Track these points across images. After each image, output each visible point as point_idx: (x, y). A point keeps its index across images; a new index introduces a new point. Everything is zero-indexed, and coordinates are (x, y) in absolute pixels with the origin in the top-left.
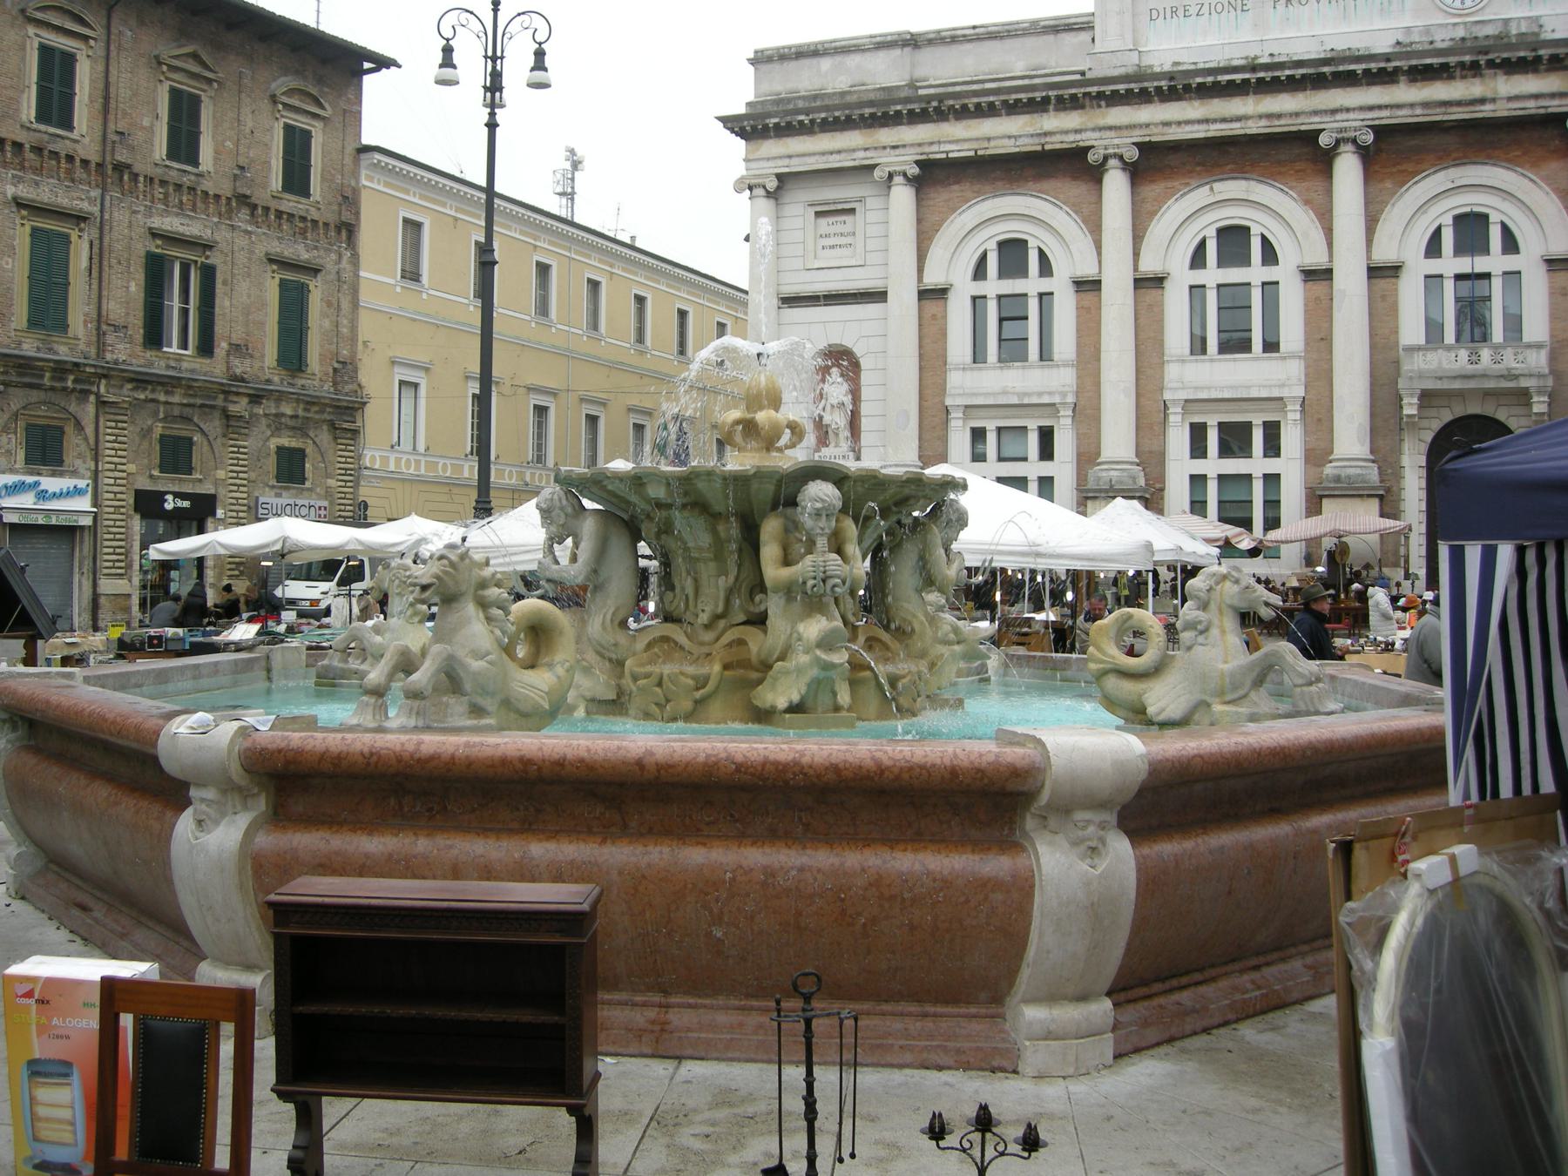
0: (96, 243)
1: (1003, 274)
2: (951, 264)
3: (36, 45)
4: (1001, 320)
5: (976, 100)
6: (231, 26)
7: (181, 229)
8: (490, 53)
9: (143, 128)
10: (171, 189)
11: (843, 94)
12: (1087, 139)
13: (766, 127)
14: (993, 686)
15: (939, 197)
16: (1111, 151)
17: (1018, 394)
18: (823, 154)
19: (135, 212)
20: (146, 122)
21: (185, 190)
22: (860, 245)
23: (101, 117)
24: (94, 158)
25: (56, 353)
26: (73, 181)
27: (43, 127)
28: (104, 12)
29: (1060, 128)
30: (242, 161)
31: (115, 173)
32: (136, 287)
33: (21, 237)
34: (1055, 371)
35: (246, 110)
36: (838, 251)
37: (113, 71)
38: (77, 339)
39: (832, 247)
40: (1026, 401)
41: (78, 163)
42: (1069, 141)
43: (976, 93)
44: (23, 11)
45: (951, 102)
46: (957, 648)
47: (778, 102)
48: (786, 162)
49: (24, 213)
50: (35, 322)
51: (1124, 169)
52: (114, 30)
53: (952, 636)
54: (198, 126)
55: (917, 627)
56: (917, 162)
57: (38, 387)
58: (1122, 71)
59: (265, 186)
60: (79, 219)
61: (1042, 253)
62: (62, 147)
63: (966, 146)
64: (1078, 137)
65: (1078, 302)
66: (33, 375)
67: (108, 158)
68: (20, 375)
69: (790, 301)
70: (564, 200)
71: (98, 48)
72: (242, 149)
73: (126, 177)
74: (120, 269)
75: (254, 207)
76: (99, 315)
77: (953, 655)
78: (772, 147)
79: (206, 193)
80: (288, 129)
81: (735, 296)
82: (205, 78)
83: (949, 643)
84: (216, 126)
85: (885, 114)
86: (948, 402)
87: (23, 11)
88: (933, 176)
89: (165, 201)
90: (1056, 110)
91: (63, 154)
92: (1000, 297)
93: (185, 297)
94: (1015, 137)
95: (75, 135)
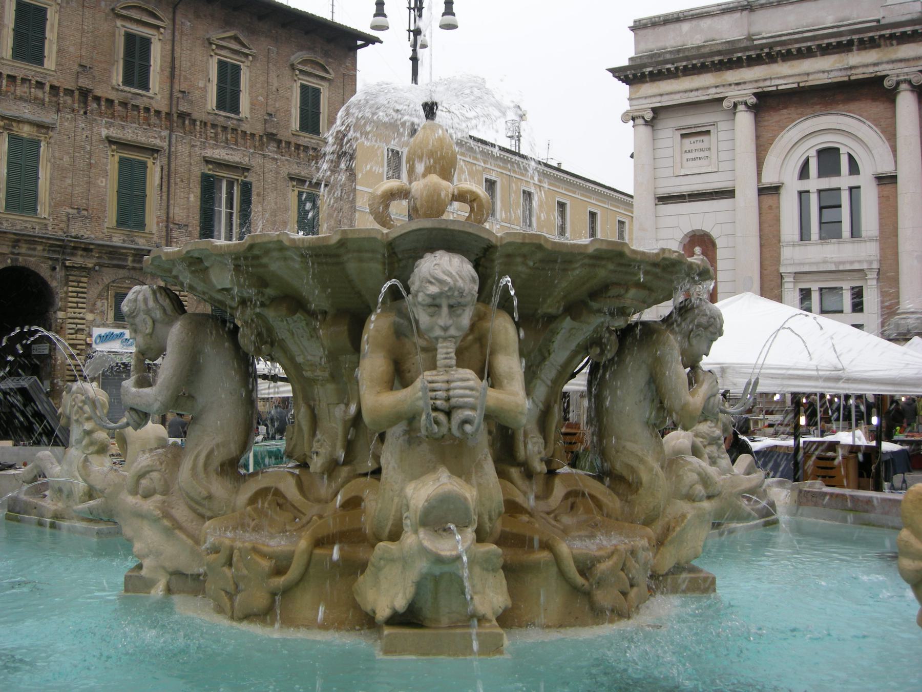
0: (166, 167)
1: (822, 174)
2: (782, 167)
3: (123, 33)
4: (821, 208)
5: (797, 46)
6: (261, 18)
7: (227, 157)
8: (413, 5)
10: (219, 130)
11: (699, 47)
12: (882, 70)
13: (643, 74)
14: (783, 535)
15: (772, 119)
16: (902, 78)
17: (835, 263)
18: (685, 92)
19: (193, 146)
20: (201, 85)
21: (230, 131)
22: (714, 157)
23: (169, 80)
24: (164, 109)
25: (137, 244)
26: (149, 125)
27: (127, 89)
28: (171, 10)
29: (862, 63)
30: (270, 110)
31: (179, 119)
32: (194, 198)
33: (112, 162)
34: (863, 244)
35: (273, 75)
36: (698, 162)
37: (178, 49)
38: (151, 233)
39: (695, 159)
40: (841, 268)
41: (152, 113)
42: (869, 72)
43: (797, 41)
44: (113, 10)
45: (779, 49)
46: (706, 505)
47: (652, 56)
48: (659, 99)
49: (114, 147)
50: (122, 222)
51: (912, 91)
52: (178, 22)
53: (699, 489)
55: (645, 477)
56: (755, 94)
57: (123, 267)
58: (908, 17)
59: (287, 127)
60: (154, 151)
61: (851, 157)
62: (141, 102)
64: (876, 69)
65: (879, 193)
66: (120, 259)
67: (174, 110)
68: (111, 259)
69: (665, 199)
71: (168, 35)
72: (270, 102)
73: (187, 122)
74: (181, 185)
75: (280, 142)
76: (168, 217)
77: (700, 516)
78: (648, 89)
79: (244, 133)
80: (304, 88)
81: (623, 199)
82: (243, 53)
83: (690, 498)
84: (251, 87)
85: (730, 60)
86: (782, 270)
87: (113, 10)
88: (767, 103)
89: (216, 138)
90: (859, 49)
91: (142, 106)
92: (820, 191)
93: (230, 205)
94: (828, 72)
95: (151, 93)
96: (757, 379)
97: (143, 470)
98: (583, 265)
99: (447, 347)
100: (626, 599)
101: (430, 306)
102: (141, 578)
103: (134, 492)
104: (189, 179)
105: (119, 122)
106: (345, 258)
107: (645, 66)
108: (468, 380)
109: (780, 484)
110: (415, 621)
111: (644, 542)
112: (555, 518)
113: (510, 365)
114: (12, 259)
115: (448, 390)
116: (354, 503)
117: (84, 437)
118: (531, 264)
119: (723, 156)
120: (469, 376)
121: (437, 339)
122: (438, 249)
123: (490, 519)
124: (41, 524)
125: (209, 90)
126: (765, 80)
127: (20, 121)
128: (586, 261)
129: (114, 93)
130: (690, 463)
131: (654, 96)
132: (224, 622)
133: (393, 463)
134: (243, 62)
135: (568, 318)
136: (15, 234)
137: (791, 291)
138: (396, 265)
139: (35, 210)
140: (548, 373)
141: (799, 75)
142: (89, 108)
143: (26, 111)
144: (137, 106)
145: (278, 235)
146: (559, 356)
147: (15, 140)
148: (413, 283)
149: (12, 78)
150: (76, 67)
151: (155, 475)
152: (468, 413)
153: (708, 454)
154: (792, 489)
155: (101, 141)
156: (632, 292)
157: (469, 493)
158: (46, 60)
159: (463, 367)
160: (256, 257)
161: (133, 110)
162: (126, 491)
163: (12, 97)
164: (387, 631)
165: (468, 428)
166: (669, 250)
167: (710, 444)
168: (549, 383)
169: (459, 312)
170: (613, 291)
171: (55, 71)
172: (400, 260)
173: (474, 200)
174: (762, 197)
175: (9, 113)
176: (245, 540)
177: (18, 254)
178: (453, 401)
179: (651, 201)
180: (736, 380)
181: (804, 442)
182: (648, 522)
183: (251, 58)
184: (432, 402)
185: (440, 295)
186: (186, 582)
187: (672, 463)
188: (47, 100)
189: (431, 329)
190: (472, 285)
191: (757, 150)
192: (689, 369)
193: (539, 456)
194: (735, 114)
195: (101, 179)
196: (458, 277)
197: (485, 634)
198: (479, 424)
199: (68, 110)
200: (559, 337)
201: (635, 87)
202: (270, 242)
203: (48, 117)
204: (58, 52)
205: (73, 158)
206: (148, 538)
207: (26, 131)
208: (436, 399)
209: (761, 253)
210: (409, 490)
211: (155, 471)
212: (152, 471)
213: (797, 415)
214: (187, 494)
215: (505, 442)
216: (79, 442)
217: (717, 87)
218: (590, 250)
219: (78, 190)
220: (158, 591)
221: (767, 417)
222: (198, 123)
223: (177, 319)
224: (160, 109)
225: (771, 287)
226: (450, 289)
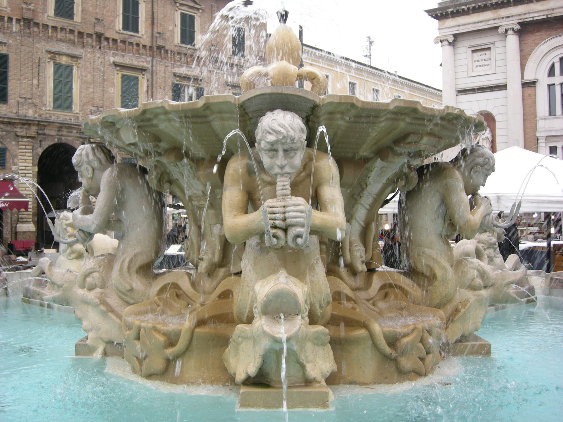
0: (150, 80)
2: (537, 70)
9: (169, 31)
14: (539, 308)
15: (530, 39)
18: (474, 23)
20: (171, 28)
23: (150, 26)
24: (148, 44)
26: (139, 54)
27: (125, 32)
31: (158, 50)
33: (117, 77)
36: (483, 68)
41: (141, 46)
46: (484, 293)
48: (457, 28)
49: (118, 68)
53: (478, 281)
54: (193, 28)
55: (439, 273)
60: (142, 70)
62: (134, 40)
63: (542, 14)
67: (154, 44)
70: (367, 58)
73: (162, 52)
77: (480, 301)
83: (473, 288)
86: (538, 135)
88: (526, 29)
91: (135, 43)
96: (520, 202)
97: (88, 271)
98: (387, 119)
99: (284, 181)
100: (424, 364)
101: (270, 150)
102: (86, 345)
103: (83, 287)
104: (165, 87)
105: (120, 53)
106: (211, 118)
107: (448, 7)
108: (299, 205)
109: (538, 274)
110: (264, 382)
111: (438, 322)
112: (374, 304)
113: (333, 193)
114: (58, 139)
115: (284, 213)
116: (226, 295)
117: (68, 248)
118: (348, 119)
119: (499, 63)
120: (300, 202)
121: (276, 175)
122: (276, 109)
123: (321, 307)
124: (42, 305)
125: (176, 31)
126: (525, 14)
127: (60, 54)
128: (389, 116)
129: (117, 35)
130: (471, 263)
131: (454, 27)
132: (135, 378)
133: (249, 267)
134: (196, 14)
135: (379, 160)
136: (59, 123)
137: (544, 146)
138: (249, 122)
139: (71, 108)
140: (367, 200)
141: (547, 10)
142: (102, 45)
143: (64, 48)
144: (132, 43)
145: (161, 103)
146: (374, 186)
147: (58, 66)
148: (257, 134)
149: (55, 28)
150: (93, 20)
151: (96, 275)
152: (299, 230)
153: (487, 255)
154: (546, 277)
155: (110, 65)
156: (425, 139)
157: (299, 290)
158: (75, 16)
159: (296, 196)
160: (150, 120)
161: (129, 45)
162: (77, 286)
163: (55, 39)
164: (243, 390)
165: (299, 241)
166: (452, 107)
167: (488, 248)
168: (368, 207)
169: (292, 154)
170: (411, 139)
171: (81, 23)
172: (251, 118)
173: (314, 78)
174: (525, 89)
175: (53, 49)
176: (147, 321)
177: (62, 135)
178: (289, 221)
179: (454, 93)
180: (507, 204)
181: (554, 245)
182: (439, 306)
183: (201, 11)
184: (272, 222)
185: (277, 142)
186: (113, 348)
187: (458, 264)
188: (76, 40)
189: (272, 168)
190: (301, 134)
191: (521, 59)
192: (470, 196)
193: (361, 260)
194: (506, 36)
195: (111, 88)
196: (289, 129)
197: (315, 392)
198: (306, 238)
199: (89, 47)
200: (373, 173)
201: (442, 22)
202: (157, 108)
203: (77, 51)
204: (82, 11)
205: (93, 76)
206: (93, 317)
207: (64, 60)
208: (275, 219)
209: (524, 125)
210: (257, 287)
211: (95, 272)
212: (93, 272)
213: (548, 226)
214: (117, 287)
215: (333, 250)
216: (65, 251)
217: (494, 19)
218: (391, 107)
219: (96, 95)
220: (98, 355)
221: (529, 228)
222: (169, 52)
223: (109, 167)
224: (146, 44)
225: (531, 143)
226: (284, 137)
